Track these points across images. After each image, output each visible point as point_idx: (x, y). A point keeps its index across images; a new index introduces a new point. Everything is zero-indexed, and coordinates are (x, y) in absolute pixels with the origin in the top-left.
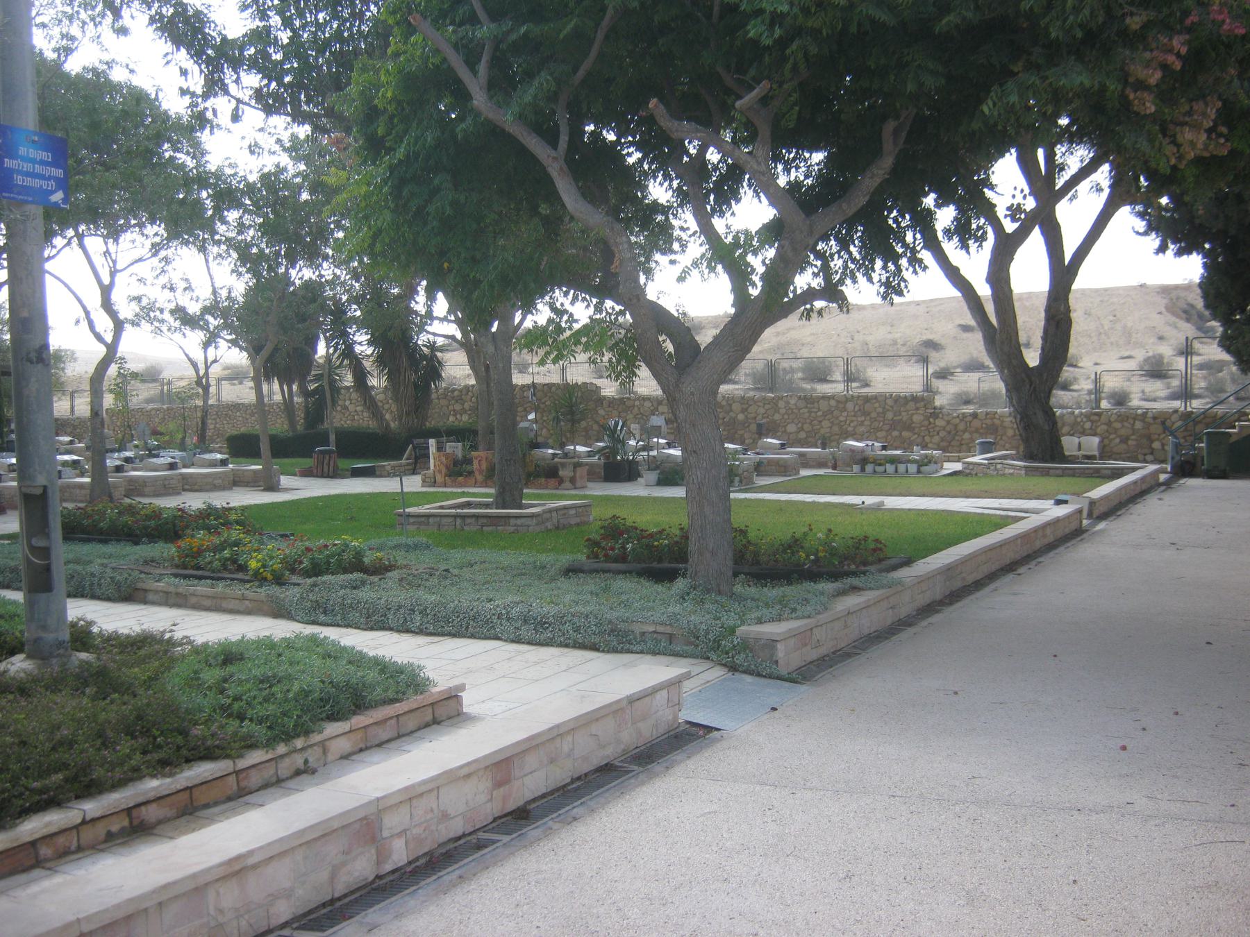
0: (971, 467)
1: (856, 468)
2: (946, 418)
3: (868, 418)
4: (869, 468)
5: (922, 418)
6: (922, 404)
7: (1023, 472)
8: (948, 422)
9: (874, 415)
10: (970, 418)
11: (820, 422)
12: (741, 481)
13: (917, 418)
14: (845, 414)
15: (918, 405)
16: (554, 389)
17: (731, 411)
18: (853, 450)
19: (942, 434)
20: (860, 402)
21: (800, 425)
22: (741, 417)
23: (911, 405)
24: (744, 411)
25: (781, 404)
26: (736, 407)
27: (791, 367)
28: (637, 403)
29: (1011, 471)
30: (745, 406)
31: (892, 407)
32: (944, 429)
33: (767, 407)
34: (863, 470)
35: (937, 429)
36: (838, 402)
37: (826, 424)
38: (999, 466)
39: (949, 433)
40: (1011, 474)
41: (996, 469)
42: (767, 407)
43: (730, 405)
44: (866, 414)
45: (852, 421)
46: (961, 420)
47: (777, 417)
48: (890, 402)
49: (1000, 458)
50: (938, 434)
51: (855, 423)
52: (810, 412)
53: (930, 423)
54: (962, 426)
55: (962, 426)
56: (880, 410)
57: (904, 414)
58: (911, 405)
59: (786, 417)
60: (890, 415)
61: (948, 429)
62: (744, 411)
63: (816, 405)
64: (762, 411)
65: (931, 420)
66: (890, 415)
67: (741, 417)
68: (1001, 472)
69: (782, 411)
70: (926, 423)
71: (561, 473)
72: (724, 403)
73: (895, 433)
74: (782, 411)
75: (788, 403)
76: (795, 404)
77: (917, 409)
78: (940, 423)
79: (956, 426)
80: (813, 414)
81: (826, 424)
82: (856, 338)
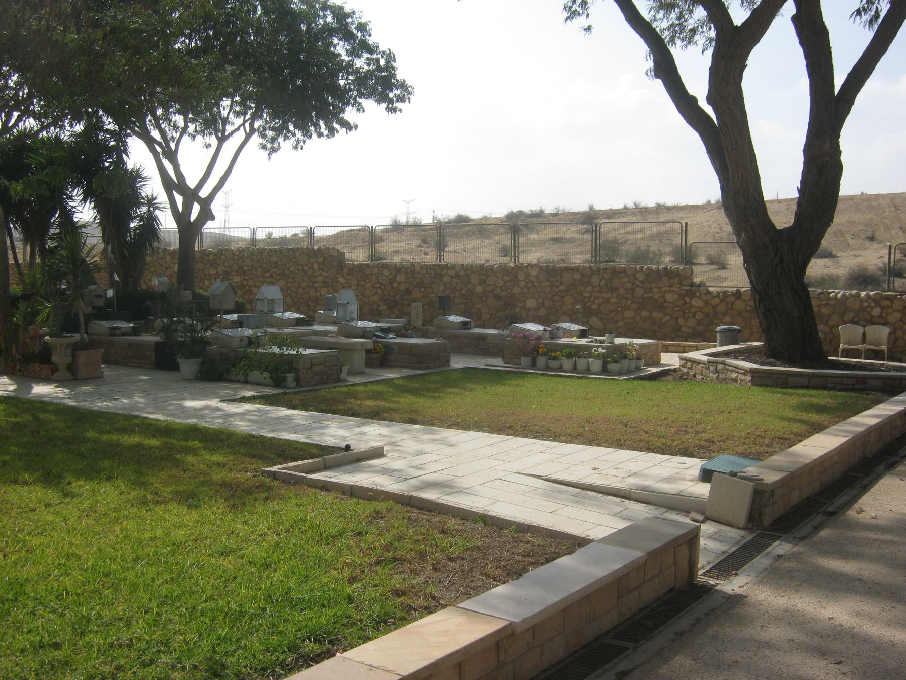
0: (689, 364)
1: (525, 361)
2: (705, 298)
3: (615, 295)
4: (541, 361)
5: (676, 296)
6: (677, 280)
7: (749, 378)
8: (706, 303)
9: (622, 291)
10: (732, 299)
11: (562, 297)
12: (297, 380)
13: (670, 297)
14: (590, 289)
15: (672, 281)
16: (298, 254)
17: (469, 282)
18: (527, 335)
19: (699, 316)
20: (607, 276)
21: (540, 300)
22: (479, 289)
23: (665, 279)
24: (482, 282)
25: (521, 276)
26: (474, 278)
27: (659, 251)
28: (376, 271)
29: (734, 375)
30: (483, 277)
31: (642, 282)
32: (701, 310)
33: (507, 278)
34: (533, 365)
35: (693, 310)
36: (583, 275)
37: (568, 300)
38: (720, 367)
39: (707, 315)
40: (735, 380)
41: (717, 371)
42: (507, 278)
43: (468, 276)
44: (613, 289)
45: (597, 298)
46: (721, 301)
47: (516, 290)
48: (640, 276)
49: (727, 354)
50: (694, 316)
51: (601, 299)
52: (551, 286)
53: (685, 303)
54: (721, 308)
55: (721, 308)
56: (629, 285)
57: (656, 290)
58: (665, 279)
59: (526, 290)
60: (639, 292)
61: (706, 310)
62: (482, 282)
63: (558, 277)
64: (501, 283)
65: (687, 299)
66: (639, 292)
67: (479, 289)
68: (722, 376)
69: (523, 284)
70: (681, 303)
71: (55, 358)
72: (462, 273)
73: (645, 313)
74: (523, 284)
75: (528, 275)
76: (536, 276)
77: (671, 286)
78: (697, 303)
79: (715, 307)
80: (555, 289)
81: (568, 300)
82: (724, 229)
